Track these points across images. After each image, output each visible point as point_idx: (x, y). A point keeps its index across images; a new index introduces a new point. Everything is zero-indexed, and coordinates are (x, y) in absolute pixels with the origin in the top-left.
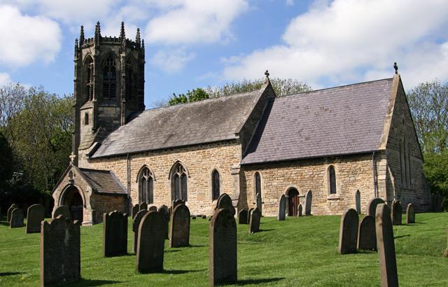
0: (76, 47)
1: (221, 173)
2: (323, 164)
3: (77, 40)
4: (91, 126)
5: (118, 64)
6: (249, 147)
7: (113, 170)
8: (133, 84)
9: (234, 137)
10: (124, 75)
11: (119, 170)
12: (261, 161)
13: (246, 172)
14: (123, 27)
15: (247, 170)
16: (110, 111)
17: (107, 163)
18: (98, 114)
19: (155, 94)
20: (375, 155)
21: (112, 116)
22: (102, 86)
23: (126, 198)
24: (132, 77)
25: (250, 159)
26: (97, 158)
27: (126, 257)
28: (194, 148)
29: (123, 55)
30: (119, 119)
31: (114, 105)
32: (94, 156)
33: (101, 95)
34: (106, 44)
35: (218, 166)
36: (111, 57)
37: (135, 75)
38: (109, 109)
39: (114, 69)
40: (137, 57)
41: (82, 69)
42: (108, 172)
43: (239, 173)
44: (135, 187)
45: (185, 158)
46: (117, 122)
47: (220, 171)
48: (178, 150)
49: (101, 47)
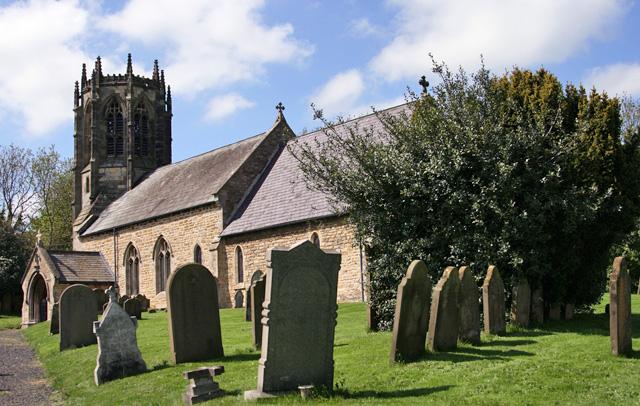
0: (77, 92)
1: (203, 250)
2: (305, 231)
3: (77, 83)
4: (89, 195)
5: (124, 109)
6: (233, 210)
7: (103, 251)
8: (149, 135)
9: (213, 199)
10: (129, 123)
11: (105, 246)
12: (241, 231)
13: (227, 248)
14: (130, 60)
15: (228, 244)
16: (115, 173)
17: (98, 242)
18: (100, 178)
19: (186, 145)
20: (209, 206)
21: (117, 179)
22: (104, 142)
23: (114, 285)
24: (148, 126)
25: (236, 227)
26: (87, 236)
27: (145, 375)
28: (176, 217)
29: (129, 97)
30: (124, 182)
31: (120, 165)
32: (88, 232)
33: (104, 152)
34: (108, 85)
35: (200, 239)
36: (115, 102)
37: (152, 123)
38: (112, 170)
39: (120, 115)
40: (153, 99)
41: (84, 120)
42: (97, 254)
43: (218, 249)
44: (122, 271)
45: (170, 230)
46: (123, 186)
47: (201, 245)
48: (162, 221)
49: (102, 89)
